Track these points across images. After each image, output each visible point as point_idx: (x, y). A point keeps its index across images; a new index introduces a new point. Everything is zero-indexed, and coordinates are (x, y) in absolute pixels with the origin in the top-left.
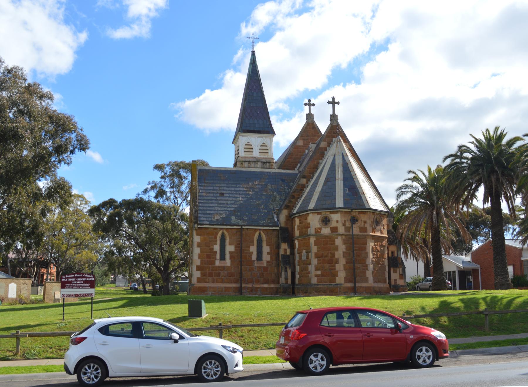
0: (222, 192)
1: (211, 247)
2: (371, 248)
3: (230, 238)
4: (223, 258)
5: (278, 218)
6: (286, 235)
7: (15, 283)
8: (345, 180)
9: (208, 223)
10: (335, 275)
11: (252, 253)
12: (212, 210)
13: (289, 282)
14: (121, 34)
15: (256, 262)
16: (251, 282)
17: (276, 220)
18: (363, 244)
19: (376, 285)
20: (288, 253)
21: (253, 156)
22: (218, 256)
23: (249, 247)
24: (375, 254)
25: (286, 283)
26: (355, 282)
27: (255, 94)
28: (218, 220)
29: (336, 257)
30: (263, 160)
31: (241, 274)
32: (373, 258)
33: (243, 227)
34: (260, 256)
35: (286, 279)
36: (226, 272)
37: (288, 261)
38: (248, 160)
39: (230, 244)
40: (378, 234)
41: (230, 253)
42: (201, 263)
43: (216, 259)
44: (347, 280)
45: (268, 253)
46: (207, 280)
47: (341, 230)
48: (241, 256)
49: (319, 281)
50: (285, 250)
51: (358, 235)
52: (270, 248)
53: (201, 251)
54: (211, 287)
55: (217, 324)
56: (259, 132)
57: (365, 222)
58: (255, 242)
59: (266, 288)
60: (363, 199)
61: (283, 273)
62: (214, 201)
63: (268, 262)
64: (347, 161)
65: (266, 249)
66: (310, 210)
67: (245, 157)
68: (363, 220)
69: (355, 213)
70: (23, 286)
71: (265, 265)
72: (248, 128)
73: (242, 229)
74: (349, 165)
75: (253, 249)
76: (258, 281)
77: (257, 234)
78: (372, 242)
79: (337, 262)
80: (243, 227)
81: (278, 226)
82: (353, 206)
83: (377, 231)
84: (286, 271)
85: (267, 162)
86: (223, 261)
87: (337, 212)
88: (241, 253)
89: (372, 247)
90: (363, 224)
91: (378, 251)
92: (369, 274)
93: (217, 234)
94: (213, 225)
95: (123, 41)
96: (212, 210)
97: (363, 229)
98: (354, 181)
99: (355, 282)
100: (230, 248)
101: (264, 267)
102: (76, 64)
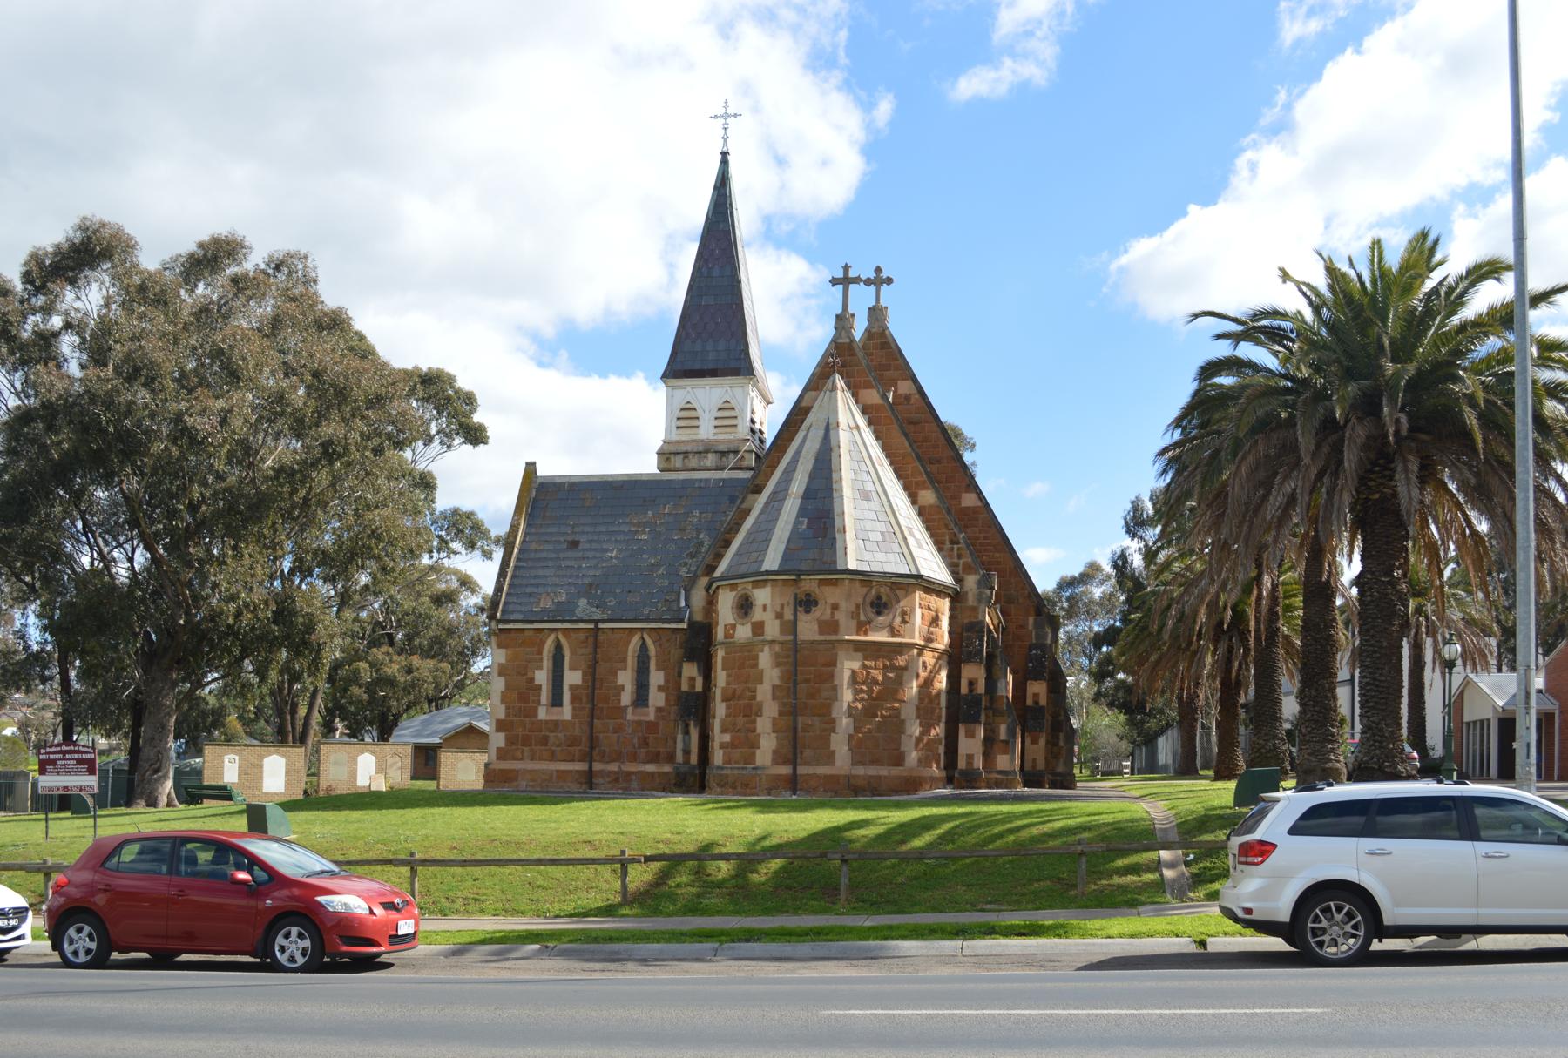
0: (577, 537)
1: (530, 675)
2: (847, 675)
3: (573, 653)
4: (556, 701)
5: (687, 599)
6: (698, 642)
7: (372, 753)
8: (808, 495)
9: (520, 617)
10: (754, 745)
11: (622, 688)
12: (538, 586)
13: (694, 759)
14: (972, 85)
15: (630, 710)
16: (618, 757)
17: (683, 604)
18: (825, 665)
19: (860, 771)
20: (699, 688)
21: (700, 437)
22: (545, 697)
23: (616, 674)
24: (862, 691)
25: (687, 761)
26: (794, 762)
27: (716, 273)
28: (545, 610)
29: (759, 698)
30: (722, 447)
31: (593, 741)
32: (855, 700)
33: (601, 626)
34: (641, 698)
35: (687, 752)
36: (561, 735)
37: (695, 708)
38: (684, 449)
39: (571, 668)
40: (882, 637)
41: (572, 687)
42: (508, 715)
43: (539, 703)
44: (778, 758)
45: (660, 689)
46: (519, 754)
47: (772, 630)
48: (595, 697)
49: (728, 761)
50: (692, 680)
51: (813, 642)
52: (666, 675)
53: (508, 686)
54: (526, 771)
55: (616, 852)
56: (713, 373)
57: (835, 607)
58: (631, 661)
59: (652, 774)
60: (839, 544)
61: (680, 737)
62: (550, 563)
63: (659, 710)
64: (833, 443)
65: (656, 678)
66: (768, 573)
67: (678, 443)
68: (831, 600)
69: (809, 584)
70: (390, 761)
71: (652, 717)
72: (688, 366)
73: (597, 629)
74: (834, 454)
75: (626, 678)
76: (634, 758)
77: (635, 642)
78: (852, 659)
79: (759, 713)
80: (601, 626)
81: (682, 621)
82: (804, 567)
83: (879, 629)
84: (687, 733)
85: (729, 452)
86: (556, 709)
87: (834, 583)
88: (594, 688)
89: (853, 672)
90: (829, 611)
91: (876, 682)
92: (840, 744)
93: (543, 643)
94: (532, 622)
95: (978, 105)
96: (538, 586)
97: (830, 626)
98: (831, 497)
99: (794, 762)
100: (573, 678)
101: (649, 723)
102: (867, 190)
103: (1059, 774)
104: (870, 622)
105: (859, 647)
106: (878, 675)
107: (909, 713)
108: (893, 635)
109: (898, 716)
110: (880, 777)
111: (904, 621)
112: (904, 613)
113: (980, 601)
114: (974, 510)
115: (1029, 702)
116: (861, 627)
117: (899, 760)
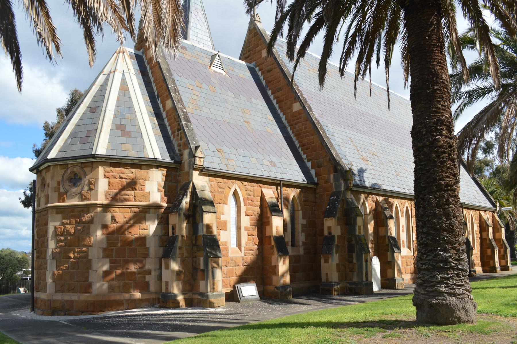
19: (59, 297)
24: (61, 241)
83: (73, 196)
103: (354, 283)
104: (66, 193)
105: (59, 210)
106: (71, 228)
107: (94, 254)
108: (83, 200)
109: (87, 256)
110: (72, 301)
111: (90, 189)
112: (90, 183)
113: (190, 168)
114: (299, 113)
115: (326, 233)
116: (61, 198)
117: (87, 288)
